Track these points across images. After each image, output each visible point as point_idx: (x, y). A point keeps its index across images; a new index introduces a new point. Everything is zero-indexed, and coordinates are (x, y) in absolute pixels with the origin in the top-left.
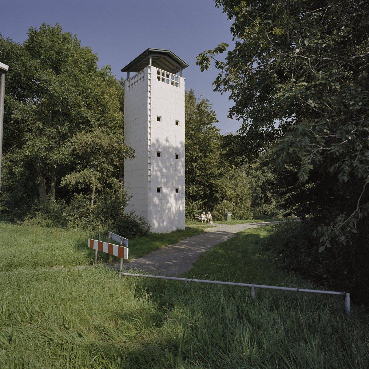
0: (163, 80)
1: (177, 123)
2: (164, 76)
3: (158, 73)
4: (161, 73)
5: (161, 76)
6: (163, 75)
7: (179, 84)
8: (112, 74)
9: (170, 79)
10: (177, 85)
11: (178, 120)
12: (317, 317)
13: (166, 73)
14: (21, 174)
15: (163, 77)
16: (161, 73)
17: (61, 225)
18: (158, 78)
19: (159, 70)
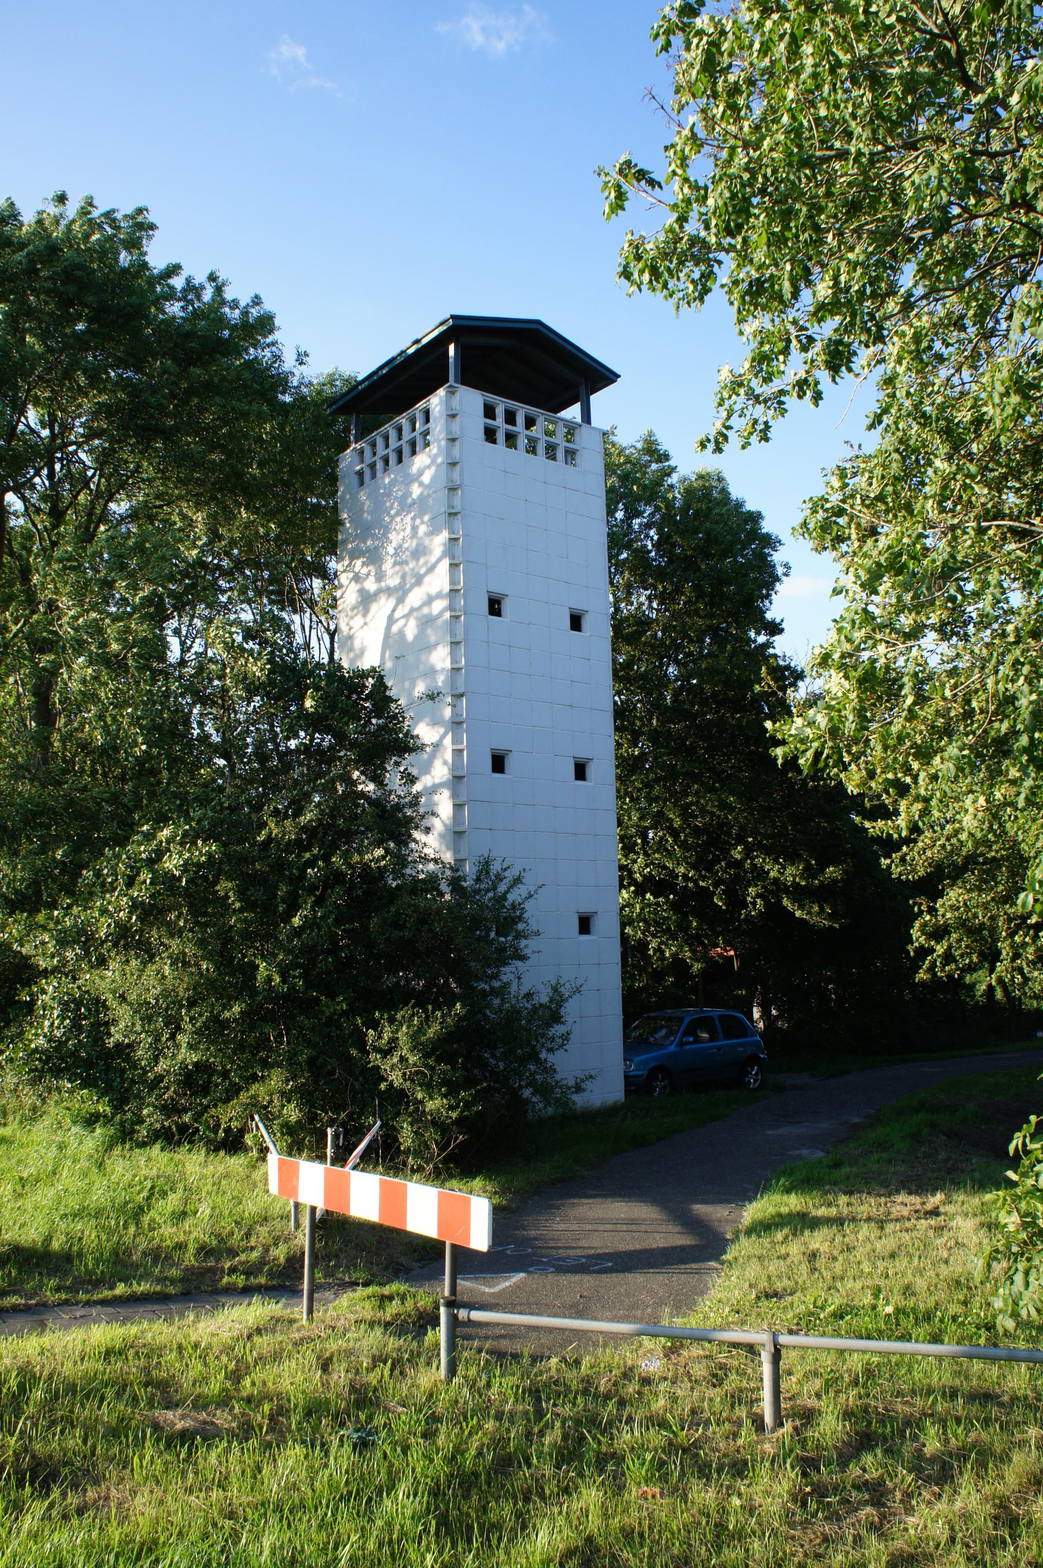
0: (511, 439)
1: (576, 622)
2: (494, 419)
3: (489, 412)
4: (520, 420)
5: (500, 422)
6: (510, 417)
7: (578, 457)
8: (784, 578)
9: (536, 431)
10: (571, 454)
11: (579, 605)
12: (646, 1529)
13: (522, 411)
14: (70, 1081)
15: (510, 427)
16: (520, 420)
17: (365, 1157)
18: (490, 435)
19: (492, 398)
